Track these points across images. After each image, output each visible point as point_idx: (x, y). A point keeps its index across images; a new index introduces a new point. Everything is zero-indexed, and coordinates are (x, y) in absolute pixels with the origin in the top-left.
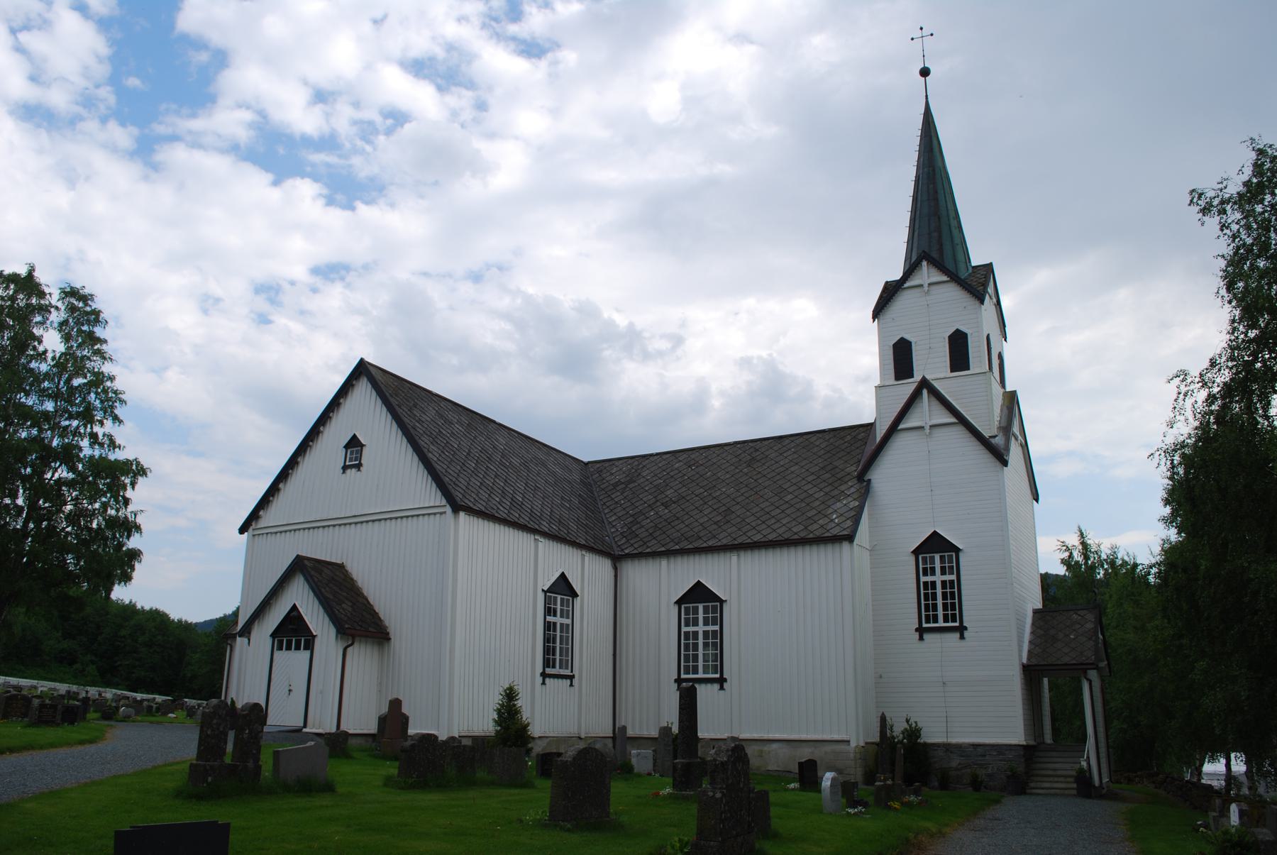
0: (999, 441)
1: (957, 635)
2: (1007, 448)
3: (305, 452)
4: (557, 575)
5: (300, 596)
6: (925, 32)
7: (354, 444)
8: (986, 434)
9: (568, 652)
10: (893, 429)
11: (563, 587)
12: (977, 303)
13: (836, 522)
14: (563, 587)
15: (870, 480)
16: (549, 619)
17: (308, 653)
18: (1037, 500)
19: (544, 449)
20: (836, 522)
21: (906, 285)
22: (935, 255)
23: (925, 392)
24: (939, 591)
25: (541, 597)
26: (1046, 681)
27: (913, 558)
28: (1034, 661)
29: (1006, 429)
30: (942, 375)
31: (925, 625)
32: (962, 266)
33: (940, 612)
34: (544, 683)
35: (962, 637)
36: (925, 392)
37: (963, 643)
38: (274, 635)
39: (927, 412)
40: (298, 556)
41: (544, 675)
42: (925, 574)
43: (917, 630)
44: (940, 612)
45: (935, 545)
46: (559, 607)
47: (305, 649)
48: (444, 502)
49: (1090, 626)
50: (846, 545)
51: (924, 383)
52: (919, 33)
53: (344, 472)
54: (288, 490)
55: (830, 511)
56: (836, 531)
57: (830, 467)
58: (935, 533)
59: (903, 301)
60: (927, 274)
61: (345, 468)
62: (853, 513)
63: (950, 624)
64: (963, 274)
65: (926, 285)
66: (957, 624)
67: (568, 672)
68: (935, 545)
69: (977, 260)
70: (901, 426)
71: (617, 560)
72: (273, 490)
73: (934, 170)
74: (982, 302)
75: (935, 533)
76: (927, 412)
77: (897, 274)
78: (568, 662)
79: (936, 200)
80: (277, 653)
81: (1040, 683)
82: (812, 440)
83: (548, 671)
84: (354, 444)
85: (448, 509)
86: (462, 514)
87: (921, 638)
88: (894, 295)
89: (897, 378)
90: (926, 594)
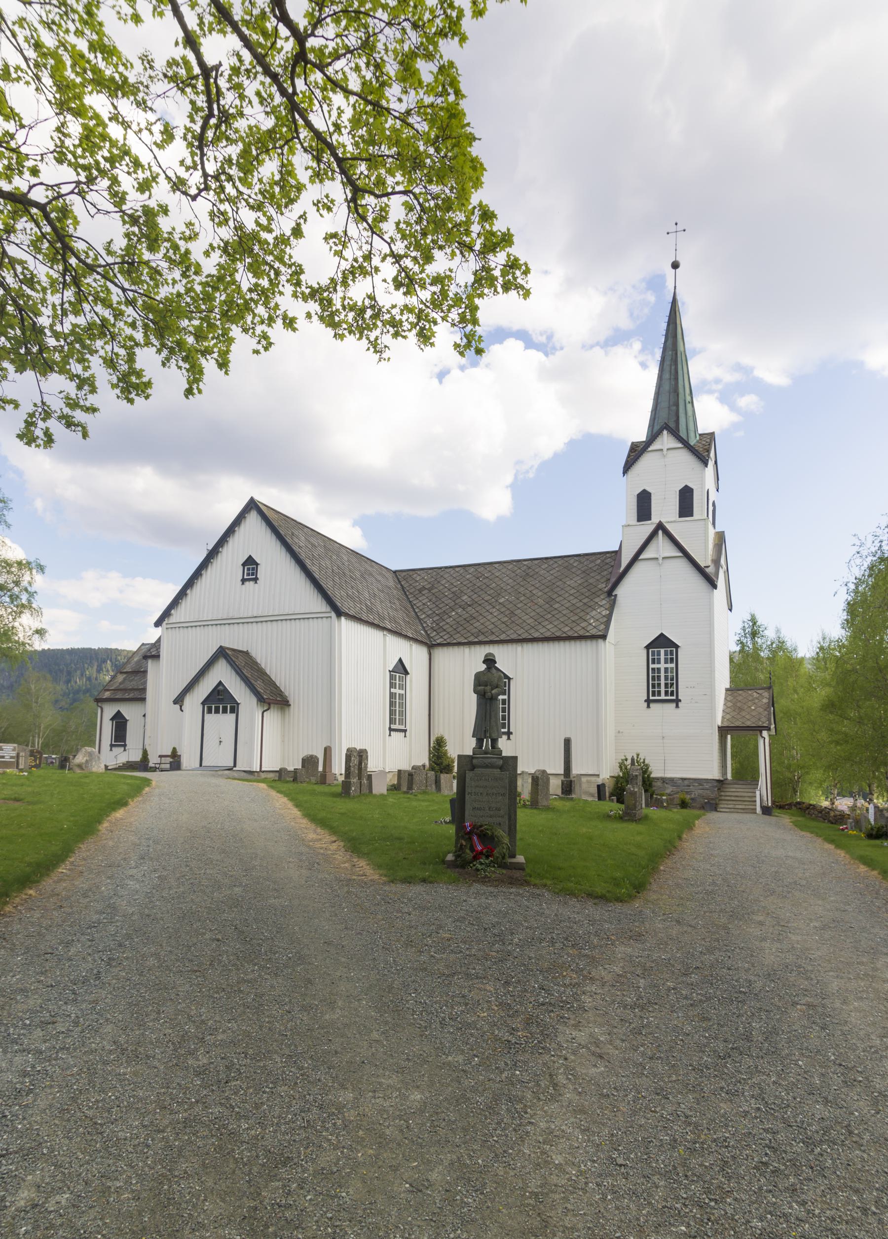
0: (710, 570)
1: (674, 705)
2: (717, 574)
3: (207, 567)
4: (397, 660)
5: (222, 674)
6: (680, 227)
7: (250, 563)
8: (702, 564)
9: (403, 713)
10: (635, 559)
11: (401, 668)
12: (702, 466)
13: (593, 626)
14: (401, 668)
15: (616, 595)
16: (393, 690)
17: (234, 715)
18: (731, 610)
19: (369, 562)
20: (593, 626)
21: (650, 449)
22: (672, 425)
23: (660, 532)
24: (662, 674)
25: (388, 674)
26: (729, 737)
27: (645, 651)
28: (726, 724)
29: (717, 562)
30: (673, 519)
31: (651, 698)
32: (692, 434)
33: (663, 689)
34: (390, 735)
35: (677, 706)
36: (660, 532)
37: (678, 711)
38: (203, 703)
39: (661, 547)
40: (221, 647)
41: (391, 730)
42: (653, 662)
43: (645, 701)
44: (663, 689)
45: (662, 642)
46: (397, 682)
47: (231, 712)
48: (329, 609)
49: (765, 701)
50: (600, 641)
51: (660, 526)
52: (674, 228)
53: (243, 584)
54: (194, 594)
55: (588, 617)
56: (594, 632)
57: (586, 584)
58: (662, 635)
59: (646, 461)
60: (666, 441)
61: (243, 581)
62: (605, 619)
63: (669, 698)
64: (693, 442)
65: (665, 450)
66: (674, 698)
67: (403, 727)
68: (662, 642)
69: (704, 426)
70: (641, 557)
71: (431, 646)
72: (182, 594)
73: (676, 354)
74: (706, 464)
75: (662, 635)
76: (661, 546)
77: (641, 436)
78: (402, 721)
79: (676, 379)
80: (207, 716)
81: (726, 738)
82: (571, 561)
83: (393, 727)
84: (250, 563)
85: (333, 615)
86: (343, 618)
87: (648, 706)
88: (640, 456)
89: (639, 520)
90: (652, 678)
